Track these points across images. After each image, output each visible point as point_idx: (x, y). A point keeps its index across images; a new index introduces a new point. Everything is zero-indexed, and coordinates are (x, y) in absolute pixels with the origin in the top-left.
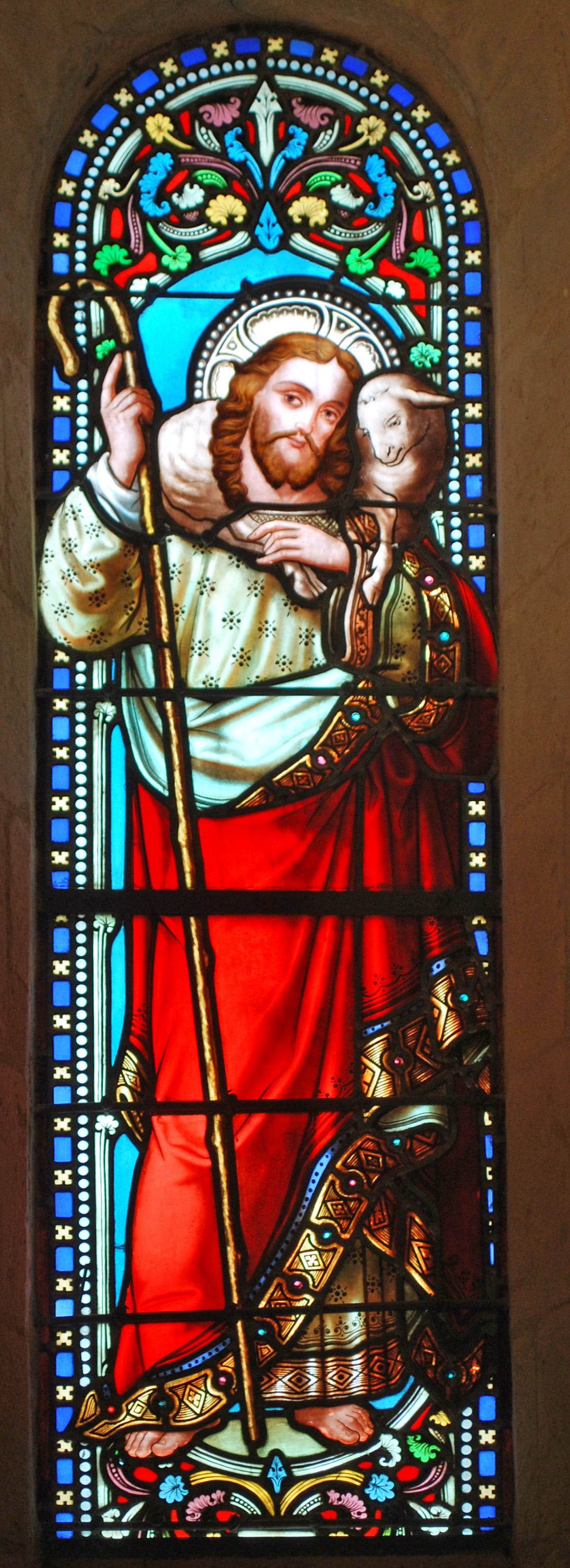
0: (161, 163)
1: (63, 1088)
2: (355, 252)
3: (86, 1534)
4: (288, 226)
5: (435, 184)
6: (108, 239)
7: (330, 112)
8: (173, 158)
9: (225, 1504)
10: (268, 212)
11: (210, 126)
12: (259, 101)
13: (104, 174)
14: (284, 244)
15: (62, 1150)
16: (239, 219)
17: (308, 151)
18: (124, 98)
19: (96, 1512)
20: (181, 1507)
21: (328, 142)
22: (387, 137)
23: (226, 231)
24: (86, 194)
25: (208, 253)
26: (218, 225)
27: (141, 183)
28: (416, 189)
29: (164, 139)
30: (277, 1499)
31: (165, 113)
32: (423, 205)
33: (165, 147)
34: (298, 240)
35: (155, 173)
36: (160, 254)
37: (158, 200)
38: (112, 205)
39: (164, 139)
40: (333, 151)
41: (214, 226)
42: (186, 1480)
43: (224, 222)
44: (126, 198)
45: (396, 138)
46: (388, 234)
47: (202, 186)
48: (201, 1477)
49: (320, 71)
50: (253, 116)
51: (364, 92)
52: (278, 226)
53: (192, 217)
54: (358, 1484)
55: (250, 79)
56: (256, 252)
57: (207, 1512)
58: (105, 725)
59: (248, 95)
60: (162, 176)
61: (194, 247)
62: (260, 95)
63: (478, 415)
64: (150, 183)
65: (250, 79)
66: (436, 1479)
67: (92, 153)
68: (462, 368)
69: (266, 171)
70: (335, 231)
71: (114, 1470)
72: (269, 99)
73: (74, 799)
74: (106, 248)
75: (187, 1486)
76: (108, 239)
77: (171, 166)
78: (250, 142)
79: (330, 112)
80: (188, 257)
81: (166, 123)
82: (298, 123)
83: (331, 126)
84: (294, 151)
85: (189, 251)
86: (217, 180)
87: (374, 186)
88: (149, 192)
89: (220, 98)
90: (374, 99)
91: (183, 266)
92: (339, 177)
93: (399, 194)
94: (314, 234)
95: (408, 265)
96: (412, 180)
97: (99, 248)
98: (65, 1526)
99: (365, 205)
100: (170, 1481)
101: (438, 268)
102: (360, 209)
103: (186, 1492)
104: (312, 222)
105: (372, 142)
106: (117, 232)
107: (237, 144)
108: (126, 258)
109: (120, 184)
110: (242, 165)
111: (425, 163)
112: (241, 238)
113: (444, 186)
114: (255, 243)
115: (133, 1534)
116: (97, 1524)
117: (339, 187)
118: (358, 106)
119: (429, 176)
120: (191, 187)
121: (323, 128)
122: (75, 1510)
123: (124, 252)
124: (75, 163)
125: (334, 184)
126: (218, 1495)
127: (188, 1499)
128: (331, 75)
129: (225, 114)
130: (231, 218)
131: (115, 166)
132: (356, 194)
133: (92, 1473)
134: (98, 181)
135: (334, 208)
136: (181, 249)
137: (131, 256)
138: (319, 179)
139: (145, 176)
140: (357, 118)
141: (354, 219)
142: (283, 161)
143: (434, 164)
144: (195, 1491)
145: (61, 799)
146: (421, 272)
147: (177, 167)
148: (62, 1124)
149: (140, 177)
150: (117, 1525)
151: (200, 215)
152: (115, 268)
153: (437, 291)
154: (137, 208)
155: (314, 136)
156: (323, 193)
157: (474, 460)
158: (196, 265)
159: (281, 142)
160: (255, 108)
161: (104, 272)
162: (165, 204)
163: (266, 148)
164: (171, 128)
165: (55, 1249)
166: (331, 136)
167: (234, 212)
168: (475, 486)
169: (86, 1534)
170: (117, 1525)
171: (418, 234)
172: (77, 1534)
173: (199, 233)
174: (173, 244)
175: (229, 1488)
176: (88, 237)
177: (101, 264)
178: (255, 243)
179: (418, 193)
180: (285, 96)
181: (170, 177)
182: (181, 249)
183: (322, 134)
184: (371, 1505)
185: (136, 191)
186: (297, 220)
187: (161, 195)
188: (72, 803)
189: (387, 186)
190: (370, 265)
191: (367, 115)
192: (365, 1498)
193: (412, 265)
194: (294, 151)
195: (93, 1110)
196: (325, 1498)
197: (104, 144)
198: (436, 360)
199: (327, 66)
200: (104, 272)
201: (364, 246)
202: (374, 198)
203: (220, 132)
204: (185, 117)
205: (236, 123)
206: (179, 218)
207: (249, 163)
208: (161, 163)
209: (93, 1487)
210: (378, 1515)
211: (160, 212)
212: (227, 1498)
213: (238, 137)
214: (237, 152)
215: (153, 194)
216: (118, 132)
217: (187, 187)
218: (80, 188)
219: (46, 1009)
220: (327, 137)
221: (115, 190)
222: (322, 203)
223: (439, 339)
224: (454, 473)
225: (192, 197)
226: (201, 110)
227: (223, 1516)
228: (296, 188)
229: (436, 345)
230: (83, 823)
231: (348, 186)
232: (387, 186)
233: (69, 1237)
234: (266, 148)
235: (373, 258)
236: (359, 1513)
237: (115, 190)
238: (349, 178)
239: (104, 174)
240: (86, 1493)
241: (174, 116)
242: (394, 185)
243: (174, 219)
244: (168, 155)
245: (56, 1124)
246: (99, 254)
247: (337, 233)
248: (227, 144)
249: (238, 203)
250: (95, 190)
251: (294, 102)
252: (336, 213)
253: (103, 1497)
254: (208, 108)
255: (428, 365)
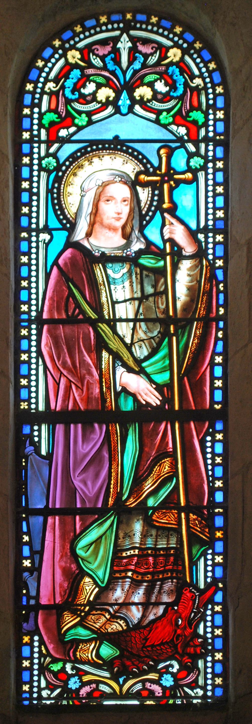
0: (76, 73)
1: (25, 217)
2: (165, 113)
3: (35, 702)
4: (133, 101)
5: (204, 79)
6: (50, 110)
7: (156, 46)
8: (81, 71)
9: (97, 689)
10: (124, 95)
11: (97, 55)
12: (122, 42)
13: (47, 80)
14: (131, 110)
15: (24, 246)
16: (111, 99)
17: (144, 65)
18: (57, 43)
19: (40, 689)
20: (78, 690)
21: (154, 60)
22: (182, 59)
23: (104, 106)
24: (39, 90)
25: (95, 118)
26: (100, 102)
27: (65, 84)
28: (194, 81)
29: (76, 62)
30: (121, 687)
31: (77, 49)
32: (197, 90)
33: (76, 66)
34: (137, 108)
35: (72, 79)
36: (75, 118)
37: (73, 92)
38: (51, 94)
39: (76, 62)
40: (158, 64)
41: (99, 102)
42: (80, 679)
43: (104, 101)
44: (58, 91)
45: (187, 58)
46: (181, 102)
47: (94, 82)
48: (86, 678)
49: (150, 27)
50: (119, 49)
51: (171, 36)
52: (129, 42)
53: (89, 98)
54: (157, 678)
55: (117, 33)
56: (118, 116)
57: (89, 694)
58: (44, 245)
59: (116, 40)
60: (75, 80)
61: (89, 114)
62: (122, 39)
63: (222, 191)
64: (69, 83)
65: (117, 33)
66: (193, 678)
67: (41, 70)
68: (213, 685)
69: (124, 73)
70: (155, 104)
71: (49, 675)
72: (126, 41)
73: (30, 305)
74: (48, 114)
75: (81, 681)
76: (50, 110)
77: (80, 75)
78: (117, 61)
79: (156, 46)
80: (87, 119)
81: (78, 55)
82: (140, 53)
83: (155, 52)
84: (137, 65)
85: (87, 116)
86: (100, 80)
87: (175, 82)
88: (69, 88)
89: (103, 42)
90: (176, 39)
91: (85, 123)
92: (158, 77)
93: (186, 85)
94: (143, 103)
95: (188, 119)
96: (192, 77)
97: (45, 113)
98: (26, 699)
99: (170, 90)
100: (73, 680)
101: (203, 120)
102: (168, 93)
103: (80, 684)
104: (145, 99)
105: (174, 61)
106: (53, 106)
107: (111, 62)
108: (57, 118)
109: (56, 84)
110: (113, 73)
111: (199, 69)
112: (110, 110)
113: (208, 80)
114: (118, 111)
115: (56, 703)
116: (40, 698)
117: (159, 81)
118: (170, 43)
119: (201, 76)
120: (89, 83)
121: (152, 54)
122: (31, 692)
123: (57, 116)
124: (34, 74)
125: (156, 80)
126: (94, 686)
127: (81, 687)
128: (155, 29)
129: (102, 51)
130: (108, 98)
131: (52, 75)
132: (166, 84)
133: (39, 676)
134: (44, 84)
135: (155, 93)
136: (84, 115)
137: (60, 116)
138: (148, 79)
139: (68, 80)
140: (168, 49)
141: (166, 98)
142: (132, 70)
143: (204, 70)
144: (84, 684)
145: (25, 257)
146: (195, 122)
147: (83, 74)
148: (26, 639)
149: (65, 81)
150: (49, 698)
151: (94, 97)
152: (52, 123)
153: (203, 132)
154: (64, 95)
155: (146, 56)
156: (151, 85)
157: (219, 656)
158: (90, 123)
159: (132, 60)
160: (119, 45)
161: (47, 126)
162: (77, 93)
163: (124, 63)
164: (79, 56)
165: (21, 217)
166: (155, 57)
167: (110, 95)
168: (220, 127)
169: (35, 702)
170: (49, 698)
171: (195, 103)
172: (31, 703)
173: (93, 106)
174: (80, 113)
175: (98, 682)
176: (39, 106)
177: (46, 121)
178: (118, 111)
179: (195, 83)
180: (133, 39)
181: (79, 80)
182: (84, 115)
183: (150, 57)
184: (164, 688)
185: (63, 87)
186: (138, 98)
187: (76, 88)
188: (29, 308)
189: (180, 80)
190: (171, 120)
191: (172, 47)
192: (161, 685)
193: (191, 119)
194: (137, 65)
195: (38, 231)
196: (144, 685)
197: (47, 66)
198: (202, 164)
199: (153, 25)
200: (47, 126)
201: (169, 111)
202: (173, 86)
203: (103, 58)
204: (86, 51)
205: (109, 53)
206: (83, 99)
207: (116, 71)
208: (76, 73)
209: (39, 681)
210: (168, 694)
211: (73, 97)
212: (97, 686)
213: (112, 59)
214: (111, 66)
215: (71, 88)
216: (53, 60)
217: (87, 83)
218: (35, 87)
219: (18, 289)
220: (153, 58)
221: (54, 87)
222: (149, 89)
223: (204, 154)
224: (209, 612)
225: (90, 88)
226: (94, 47)
227: (96, 694)
228: (138, 83)
229: (202, 157)
230: (34, 386)
231: (163, 81)
232: (180, 80)
233: (26, 384)
234: (124, 63)
235: (174, 116)
236: (159, 693)
237: (54, 87)
238: (163, 76)
239: (47, 80)
240: (36, 684)
241: (81, 51)
242: (183, 80)
243: (81, 100)
244: (78, 70)
245: (24, 563)
246: (44, 117)
247: (156, 105)
248: (107, 62)
249: (111, 91)
250: (43, 88)
251: (138, 44)
252: (156, 95)
253: (43, 684)
254: (97, 47)
255: (199, 167)
